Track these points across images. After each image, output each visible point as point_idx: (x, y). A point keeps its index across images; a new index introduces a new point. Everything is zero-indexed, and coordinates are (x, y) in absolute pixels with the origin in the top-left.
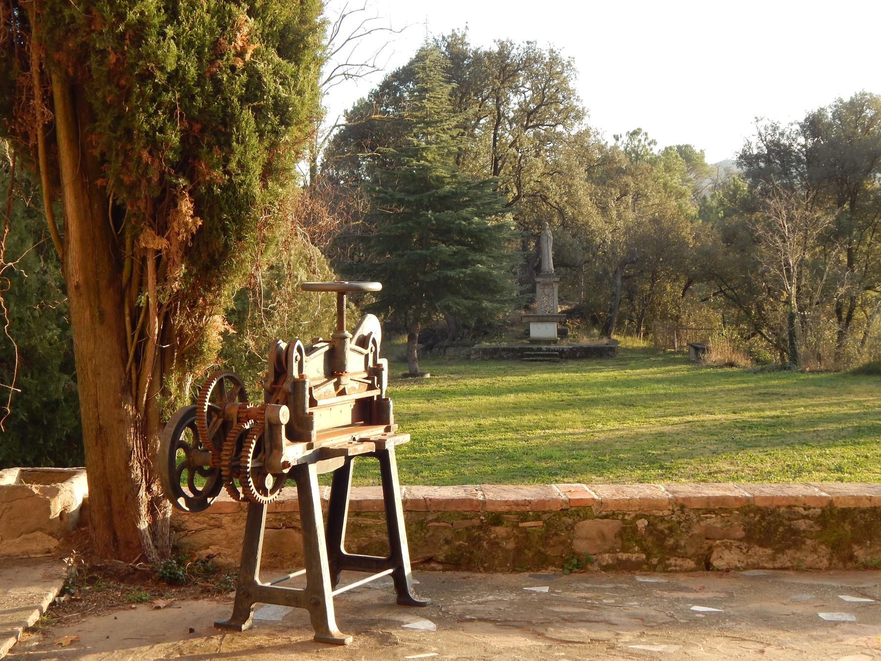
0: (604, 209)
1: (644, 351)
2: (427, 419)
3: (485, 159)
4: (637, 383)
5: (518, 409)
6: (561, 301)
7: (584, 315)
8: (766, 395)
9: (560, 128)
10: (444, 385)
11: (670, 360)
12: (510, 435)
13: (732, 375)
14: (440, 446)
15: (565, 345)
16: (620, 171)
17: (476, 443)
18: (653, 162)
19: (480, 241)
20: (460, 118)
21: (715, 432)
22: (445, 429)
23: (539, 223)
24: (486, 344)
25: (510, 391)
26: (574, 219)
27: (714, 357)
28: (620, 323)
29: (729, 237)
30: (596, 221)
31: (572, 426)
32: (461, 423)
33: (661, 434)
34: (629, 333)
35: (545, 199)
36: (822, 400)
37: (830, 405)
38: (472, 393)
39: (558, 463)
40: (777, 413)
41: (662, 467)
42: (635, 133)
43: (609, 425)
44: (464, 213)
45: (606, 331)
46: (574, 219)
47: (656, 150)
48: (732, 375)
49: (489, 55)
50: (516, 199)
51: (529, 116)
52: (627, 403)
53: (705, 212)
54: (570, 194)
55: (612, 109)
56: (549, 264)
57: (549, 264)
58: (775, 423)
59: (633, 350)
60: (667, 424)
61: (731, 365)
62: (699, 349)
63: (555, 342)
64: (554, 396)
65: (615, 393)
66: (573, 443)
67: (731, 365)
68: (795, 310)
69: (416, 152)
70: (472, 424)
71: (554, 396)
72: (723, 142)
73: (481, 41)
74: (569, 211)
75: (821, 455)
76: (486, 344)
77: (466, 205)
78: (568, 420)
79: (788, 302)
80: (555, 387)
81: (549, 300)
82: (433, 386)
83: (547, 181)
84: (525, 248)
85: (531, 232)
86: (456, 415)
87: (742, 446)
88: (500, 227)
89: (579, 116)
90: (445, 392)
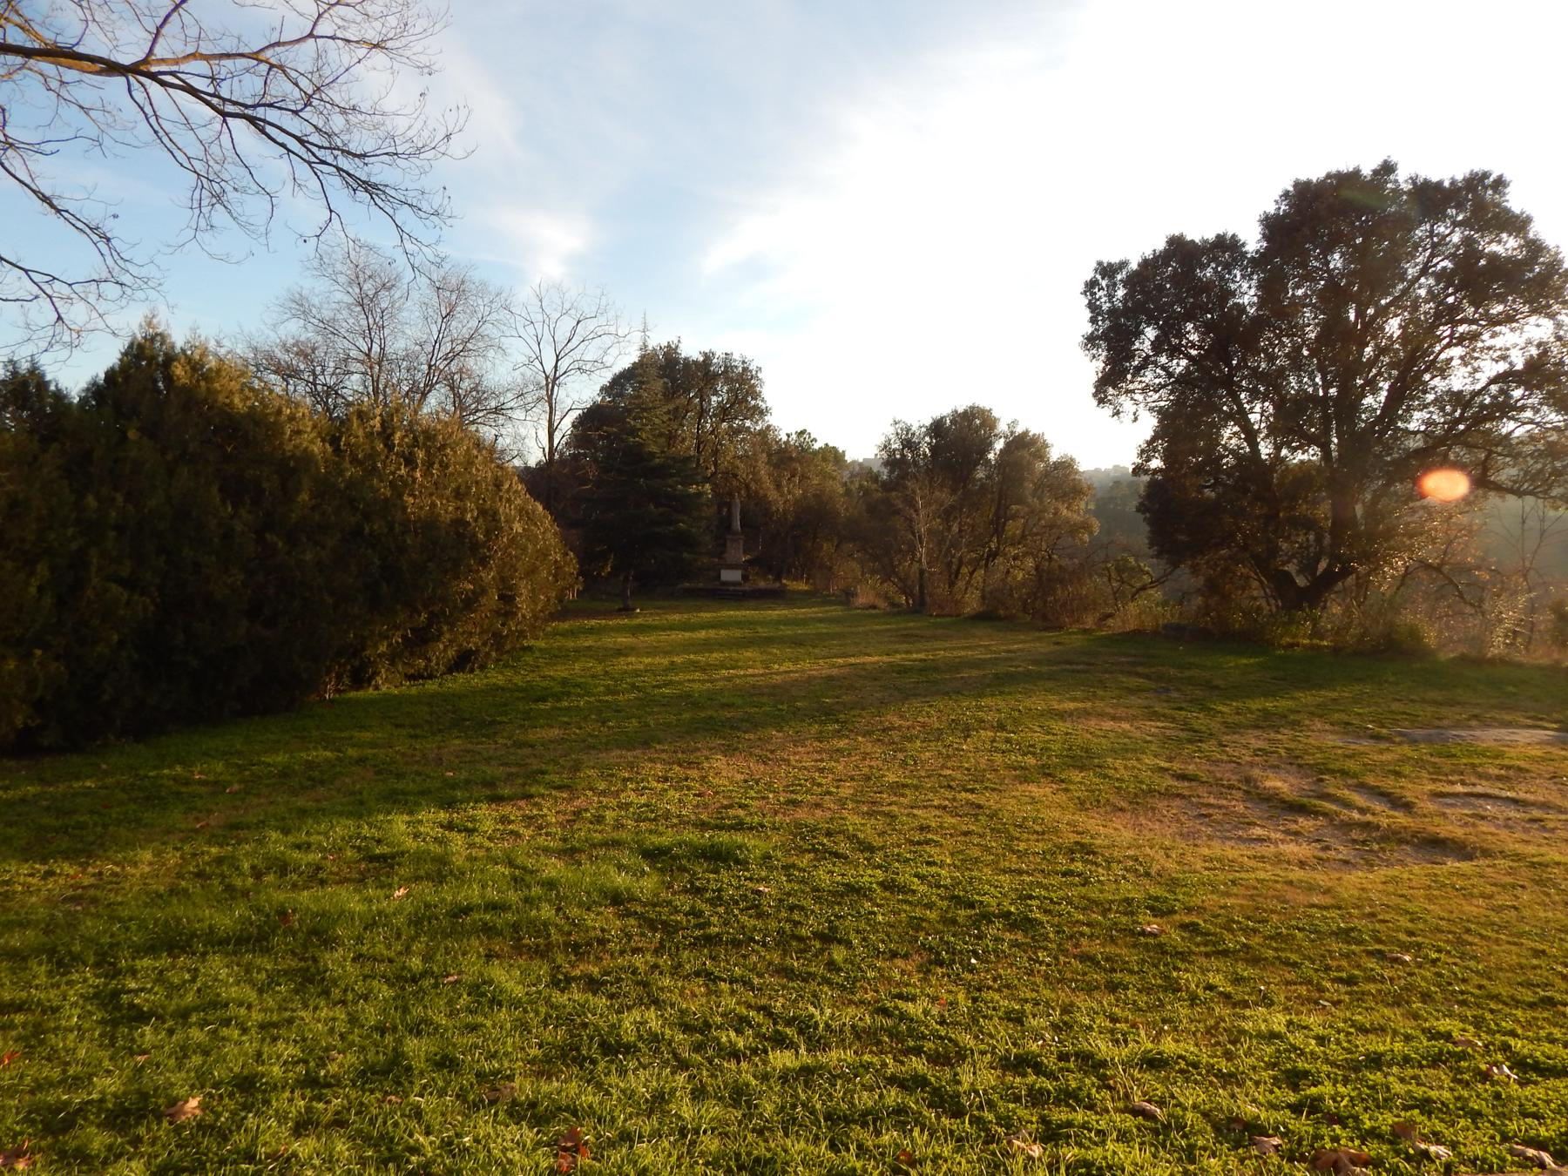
0: (778, 486)
1: (806, 592)
2: (626, 656)
3: (691, 443)
4: (803, 622)
5: (707, 646)
6: (745, 553)
7: (763, 564)
8: (907, 637)
9: (748, 423)
10: (650, 621)
11: (826, 601)
12: (697, 675)
13: (876, 616)
14: (634, 687)
15: (747, 587)
16: (791, 459)
17: (665, 685)
18: (816, 453)
19: (686, 504)
20: (671, 407)
21: (876, 675)
22: (641, 667)
23: (730, 494)
24: (687, 585)
25: (703, 626)
26: (756, 492)
27: (861, 600)
28: (789, 571)
29: (872, 509)
30: (773, 495)
31: (752, 668)
32: (657, 660)
33: (830, 678)
34: (796, 579)
35: (735, 476)
36: (955, 643)
37: (963, 648)
38: (671, 628)
39: (740, 714)
40: (922, 656)
41: (837, 721)
42: (803, 432)
43: (788, 667)
44: (670, 481)
45: (778, 578)
46: (756, 492)
47: (816, 446)
48: (876, 616)
49: (696, 363)
50: (714, 474)
51: (724, 413)
52: (797, 642)
53: (848, 493)
54: (754, 474)
55: (789, 411)
56: (737, 524)
57: (737, 524)
58: (925, 668)
59: (799, 592)
60: (833, 666)
61: (874, 607)
62: (847, 596)
63: (739, 584)
64: (738, 633)
65: (788, 631)
66: (754, 687)
67: (874, 607)
68: (925, 566)
69: (633, 432)
70: (665, 661)
71: (738, 633)
72: (862, 444)
73: (691, 350)
74: (753, 486)
75: (980, 708)
76: (687, 585)
77: (672, 475)
78: (750, 659)
79: (920, 561)
80: (739, 624)
81: (737, 553)
82: (639, 621)
83: (738, 462)
84: (719, 511)
85: (723, 500)
86: (653, 651)
87: (906, 695)
88: (699, 494)
89: (763, 413)
90: (649, 627)
